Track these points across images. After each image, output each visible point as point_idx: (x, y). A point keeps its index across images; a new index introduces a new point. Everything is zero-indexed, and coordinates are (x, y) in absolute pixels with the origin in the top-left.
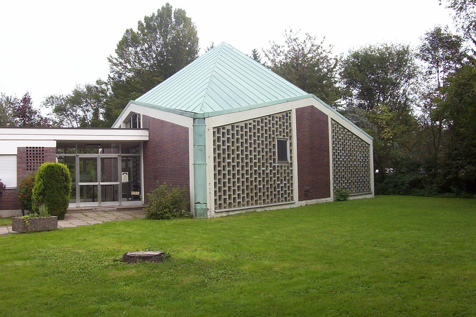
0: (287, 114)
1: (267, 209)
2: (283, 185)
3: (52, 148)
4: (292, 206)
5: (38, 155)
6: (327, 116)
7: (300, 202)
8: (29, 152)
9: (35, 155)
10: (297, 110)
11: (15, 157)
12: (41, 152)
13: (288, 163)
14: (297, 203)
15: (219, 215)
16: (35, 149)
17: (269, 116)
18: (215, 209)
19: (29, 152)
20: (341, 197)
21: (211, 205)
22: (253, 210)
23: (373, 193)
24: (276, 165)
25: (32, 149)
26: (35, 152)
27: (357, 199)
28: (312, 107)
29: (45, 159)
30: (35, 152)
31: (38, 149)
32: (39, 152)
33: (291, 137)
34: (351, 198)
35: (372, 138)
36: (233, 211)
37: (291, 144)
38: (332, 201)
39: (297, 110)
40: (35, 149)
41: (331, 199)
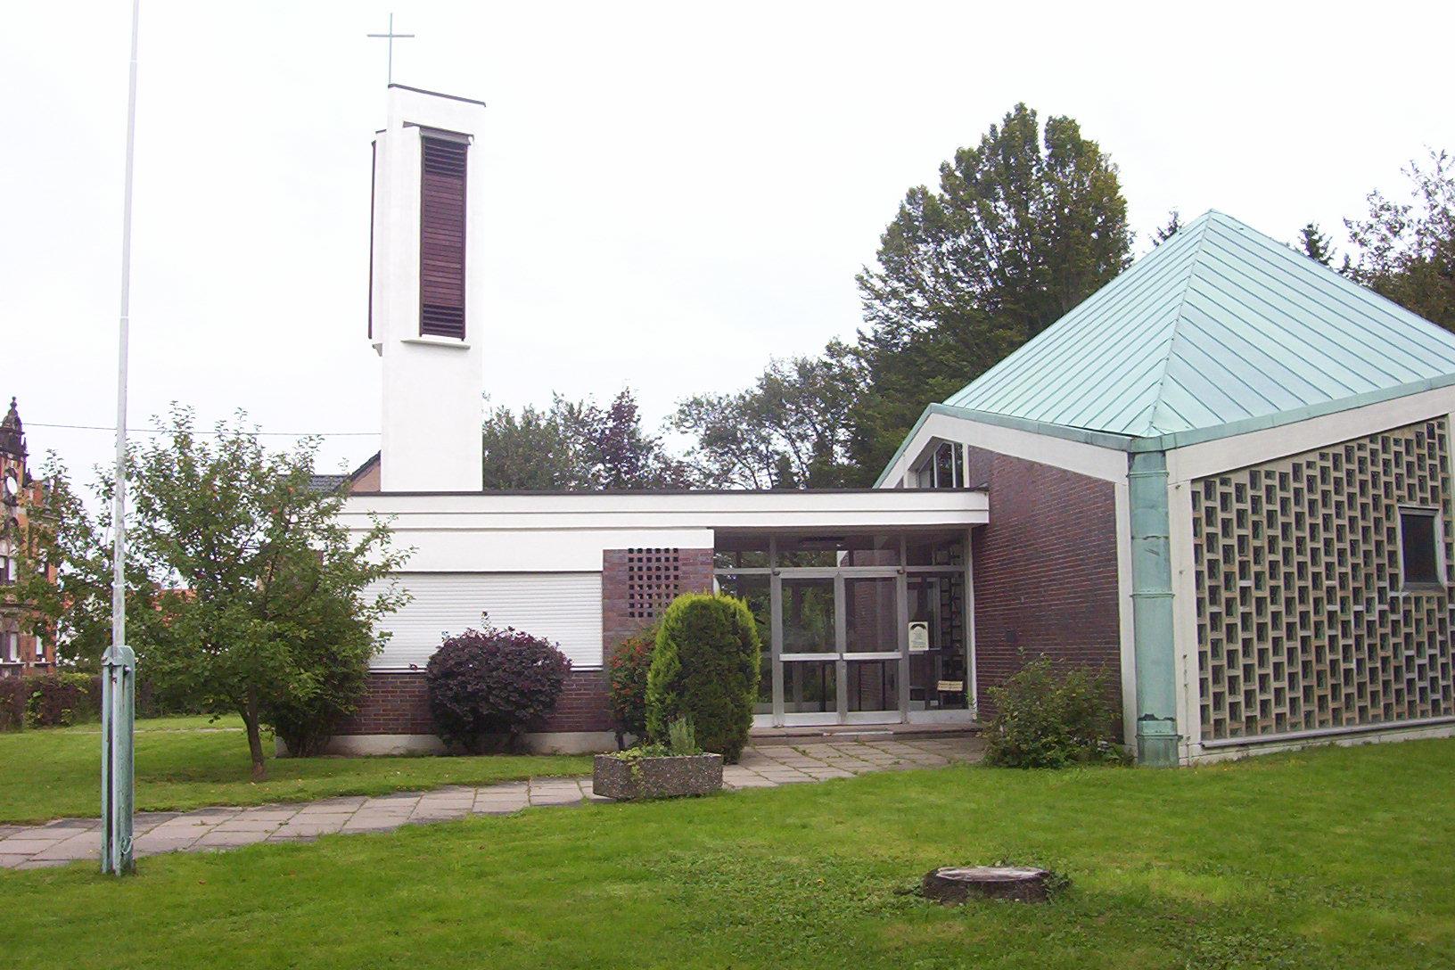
1: (1373, 739)
5: (663, 573)
8: (636, 565)
9: (654, 573)
11: (596, 584)
12: (671, 564)
13: (1440, 588)
15: (1215, 757)
17: (1372, 438)
18: (1204, 735)
19: (636, 565)
22: (1326, 742)
25: (644, 556)
26: (654, 564)
29: (680, 582)
30: (654, 564)
32: (644, 565)
36: (1262, 743)
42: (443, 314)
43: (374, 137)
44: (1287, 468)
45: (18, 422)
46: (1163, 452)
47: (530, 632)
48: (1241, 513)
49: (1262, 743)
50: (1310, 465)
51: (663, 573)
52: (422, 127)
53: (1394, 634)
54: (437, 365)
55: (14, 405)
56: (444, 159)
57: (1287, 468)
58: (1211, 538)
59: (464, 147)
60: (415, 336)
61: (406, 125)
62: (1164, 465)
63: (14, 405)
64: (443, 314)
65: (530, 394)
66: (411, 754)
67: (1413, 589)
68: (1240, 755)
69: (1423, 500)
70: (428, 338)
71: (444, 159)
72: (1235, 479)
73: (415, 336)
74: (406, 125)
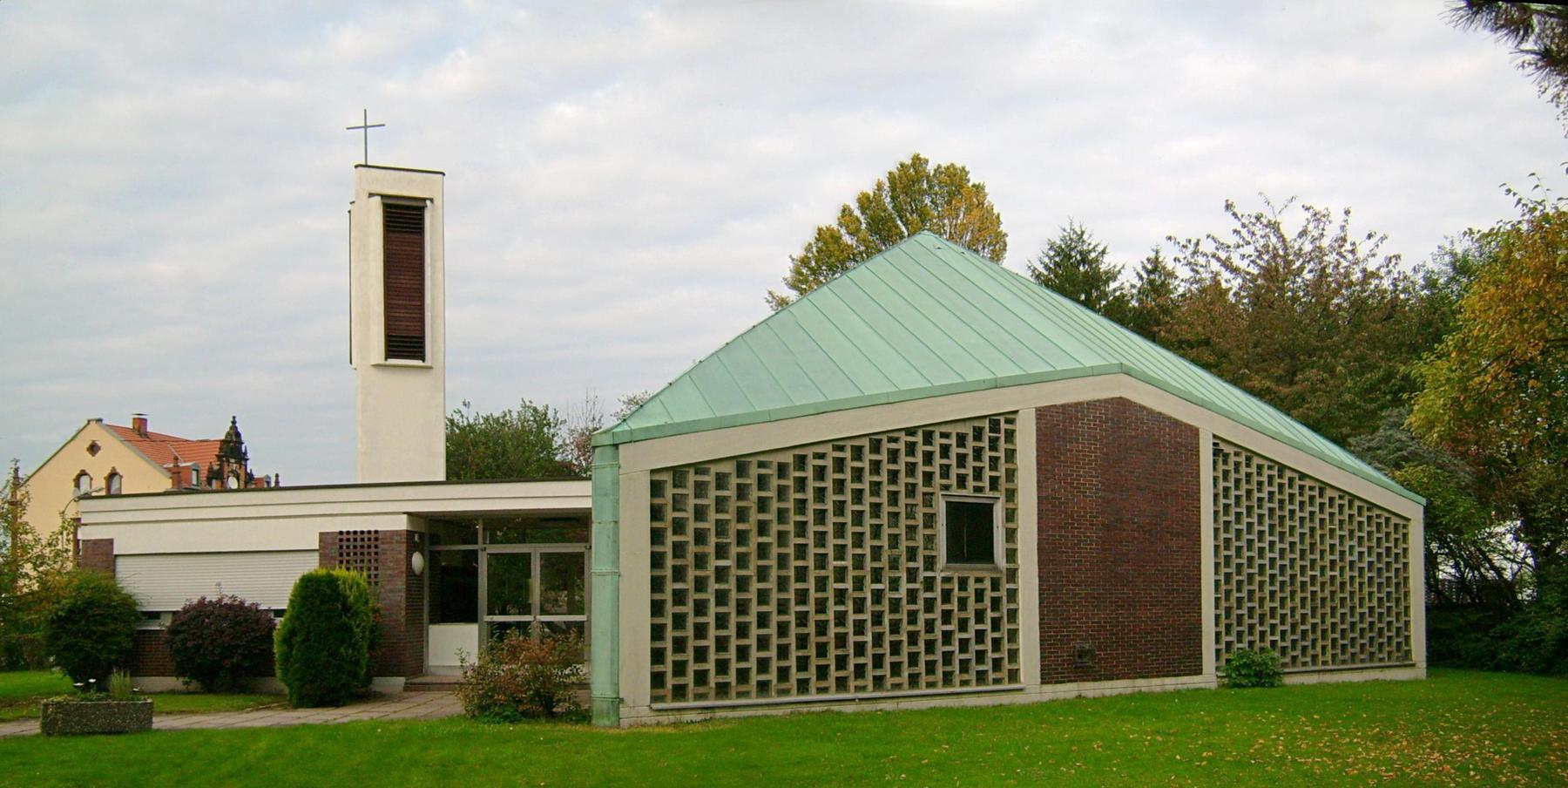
0: (999, 427)
1: (836, 708)
2: (1365, 626)
3: (397, 533)
4: (1019, 699)
5: (366, 551)
6: (1194, 432)
7: (1048, 688)
8: (345, 544)
9: (359, 550)
10: (1042, 413)
11: (317, 555)
12: (373, 543)
13: (996, 569)
14: (1031, 686)
15: (664, 719)
16: (359, 537)
17: (911, 431)
18: (655, 699)
19: (345, 544)
20: (1248, 675)
21: (636, 685)
22: (823, 708)
23: (1422, 664)
24: (939, 576)
25: (351, 537)
26: (359, 543)
27: (1337, 685)
28: (1122, 404)
29: (381, 557)
30: (359, 543)
31: (366, 536)
32: (351, 543)
33: (1011, 495)
34: (1287, 680)
35: (1424, 501)
36: (734, 707)
37: (1011, 515)
38: (1213, 686)
39: (1042, 413)
40: (359, 537)
41: (1209, 676)
42: (405, 339)
43: (350, 207)
44: (788, 458)
45: (238, 435)
46: (616, 446)
47: (241, 596)
48: (1271, 494)
49: (734, 707)
50: (822, 456)
51: (366, 551)
52: (383, 196)
53: (1380, 621)
54: (405, 382)
55: (234, 422)
56: (404, 222)
57: (788, 458)
58: (1227, 523)
59: (422, 209)
60: (382, 361)
61: (371, 195)
62: (616, 457)
63: (234, 422)
64: (405, 339)
65: (492, 399)
66: (173, 692)
67: (956, 570)
68: (702, 717)
69: (978, 489)
70: (392, 361)
71: (404, 222)
72: (714, 469)
73: (382, 361)
74: (371, 195)
